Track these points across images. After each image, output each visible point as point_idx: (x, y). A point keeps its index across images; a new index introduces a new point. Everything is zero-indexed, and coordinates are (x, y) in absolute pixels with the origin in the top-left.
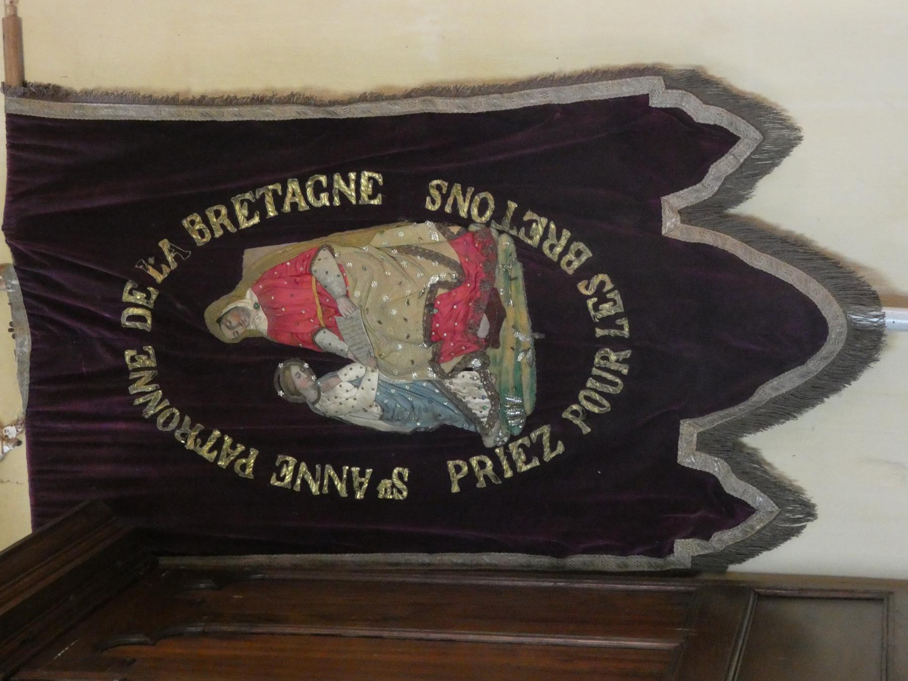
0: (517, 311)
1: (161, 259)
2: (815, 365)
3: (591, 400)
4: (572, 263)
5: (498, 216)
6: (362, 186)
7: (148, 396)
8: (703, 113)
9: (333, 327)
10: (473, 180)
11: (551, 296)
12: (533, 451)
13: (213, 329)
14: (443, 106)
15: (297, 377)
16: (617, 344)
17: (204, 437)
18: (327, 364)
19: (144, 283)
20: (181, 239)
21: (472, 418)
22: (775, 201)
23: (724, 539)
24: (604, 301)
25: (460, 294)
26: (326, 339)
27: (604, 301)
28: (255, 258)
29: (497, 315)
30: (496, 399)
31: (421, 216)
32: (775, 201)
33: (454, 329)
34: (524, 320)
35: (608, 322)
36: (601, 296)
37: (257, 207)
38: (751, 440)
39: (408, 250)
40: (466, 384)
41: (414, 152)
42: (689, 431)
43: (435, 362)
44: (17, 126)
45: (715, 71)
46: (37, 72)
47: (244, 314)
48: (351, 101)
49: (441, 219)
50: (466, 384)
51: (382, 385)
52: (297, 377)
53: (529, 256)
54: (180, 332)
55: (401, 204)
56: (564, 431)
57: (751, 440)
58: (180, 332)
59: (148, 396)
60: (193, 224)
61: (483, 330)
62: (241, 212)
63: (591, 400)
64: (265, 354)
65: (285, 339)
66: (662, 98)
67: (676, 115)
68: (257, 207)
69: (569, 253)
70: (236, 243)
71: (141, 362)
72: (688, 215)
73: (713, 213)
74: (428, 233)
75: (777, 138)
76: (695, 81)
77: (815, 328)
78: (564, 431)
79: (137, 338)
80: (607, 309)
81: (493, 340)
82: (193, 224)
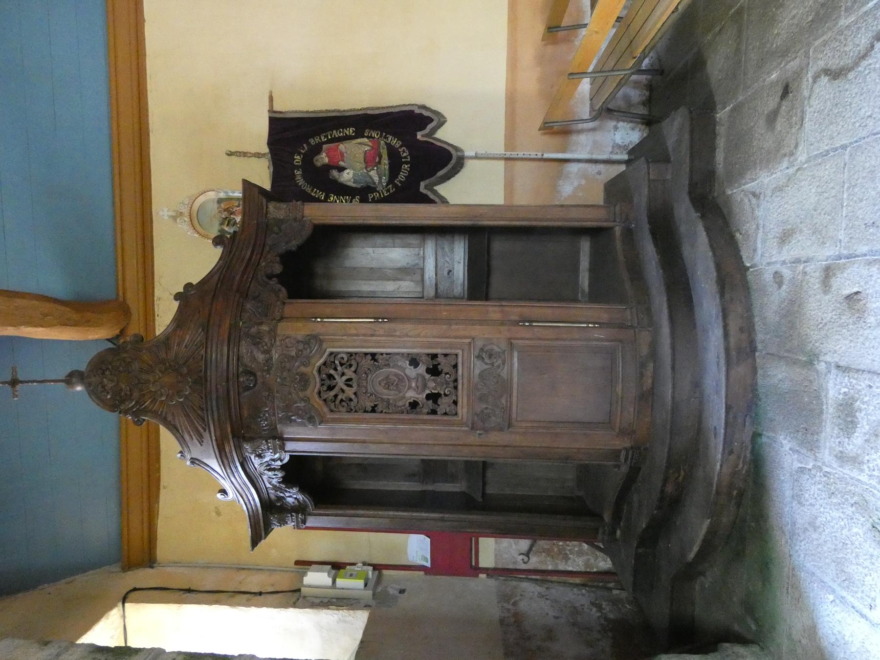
0: (385, 161)
1: (304, 148)
2: (450, 166)
3: (402, 176)
4: (398, 146)
5: (381, 136)
6: (350, 131)
7: (300, 181)
8: (426, 113)
9: (343, 161)
10: (374, 128)
11: (393, 154)
12: (388, 191)
13: (315, 163)
14: (369, 112)
15: (335, 173)
16: (407, 163)
17: (312, 190)
18: (341, 169)
19: (299, 154)
20: (309, 144)
21: (375, 183)
22: (441, 134)
23: (430, 127)
24: (405, 153)
25: (372, 152)
26: (341, 163)
27: (405, 153)
28: (325, 146)
29: (380, 157)
30: (380, 178)
31: (363, 137)
32: (441, 134)
33: (371, 161)
34: (387, 158)
35: (405, 157)
36: (404, 151)
37: (326, 136)
38: (435, 188)
39: (360, 144)
40: (373, 173)
41: (363, 122)
42: (422, 184)
43: (366, 168)
44: (271, 120)
45: (428, 106)
46: (276, 108)
47: (323, 159)
48: (347, 111)
49: (368, 137)
50: (373, 173)
51: (354, 174)
52: (335, 173)
53: (389, 145)
54: (308, 164)
55: (359, 134)
56: (395, 186)
57: (435, 188)
58: (308, 164)
59: (300, 181)
60: (312, 141)
61: (377, 160)
62: (323, 138)
63: (402, 176)
64: (327, 168)
65: (332, 164)
66: (417, 111)
67: (421, 114)
68: (326, 136)
69: (395, 142)
70: (321, 144)
71: (298, 173)
72: (422, 136)
73: (430, 187)
74: (365, 140)
75: (442, 121)
76: (424, 107)
77: (449, 156)
78: (395, 186)
79: (297, 167)
80: (405, 155)
81: (379, 162)
82: (312, 141)
